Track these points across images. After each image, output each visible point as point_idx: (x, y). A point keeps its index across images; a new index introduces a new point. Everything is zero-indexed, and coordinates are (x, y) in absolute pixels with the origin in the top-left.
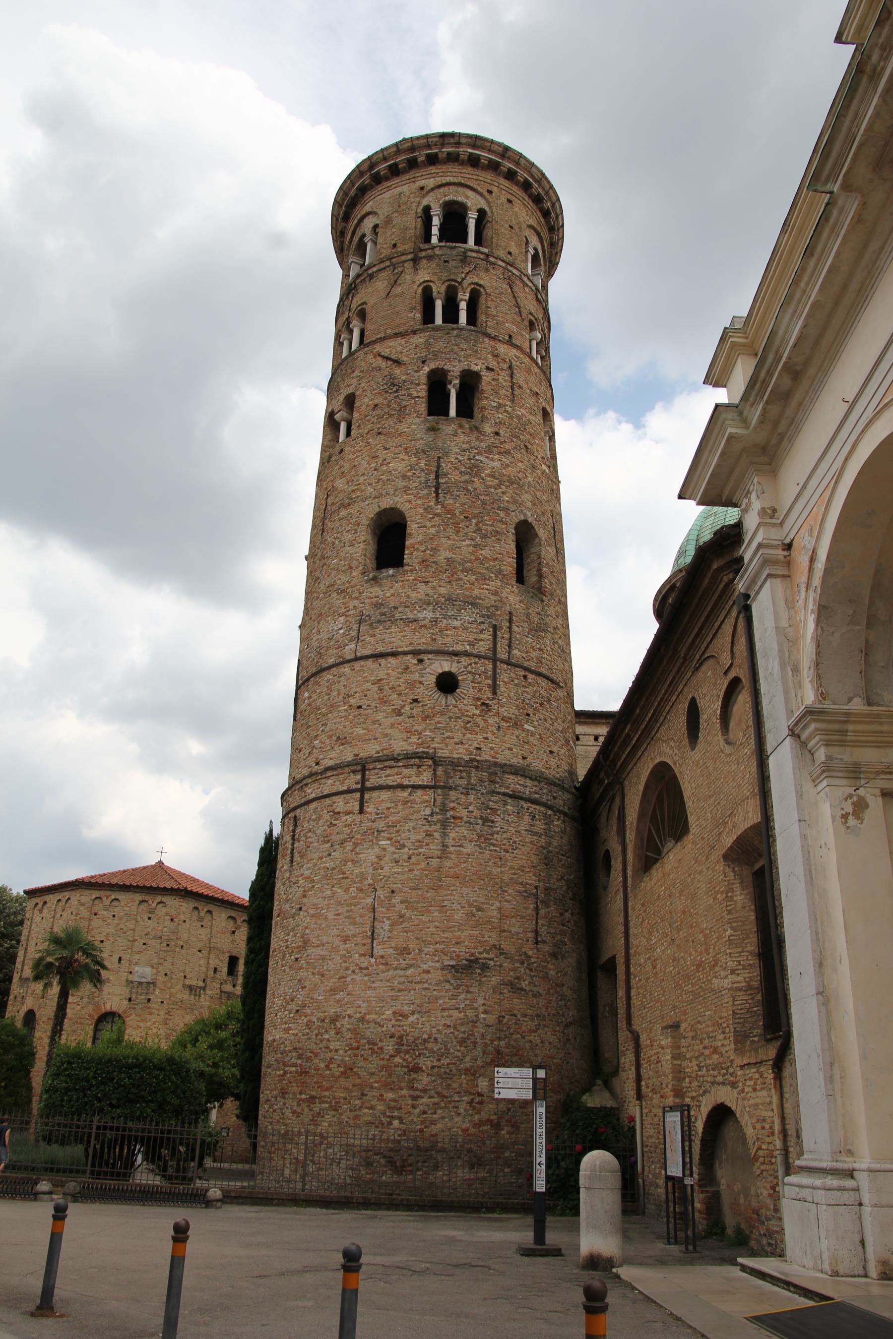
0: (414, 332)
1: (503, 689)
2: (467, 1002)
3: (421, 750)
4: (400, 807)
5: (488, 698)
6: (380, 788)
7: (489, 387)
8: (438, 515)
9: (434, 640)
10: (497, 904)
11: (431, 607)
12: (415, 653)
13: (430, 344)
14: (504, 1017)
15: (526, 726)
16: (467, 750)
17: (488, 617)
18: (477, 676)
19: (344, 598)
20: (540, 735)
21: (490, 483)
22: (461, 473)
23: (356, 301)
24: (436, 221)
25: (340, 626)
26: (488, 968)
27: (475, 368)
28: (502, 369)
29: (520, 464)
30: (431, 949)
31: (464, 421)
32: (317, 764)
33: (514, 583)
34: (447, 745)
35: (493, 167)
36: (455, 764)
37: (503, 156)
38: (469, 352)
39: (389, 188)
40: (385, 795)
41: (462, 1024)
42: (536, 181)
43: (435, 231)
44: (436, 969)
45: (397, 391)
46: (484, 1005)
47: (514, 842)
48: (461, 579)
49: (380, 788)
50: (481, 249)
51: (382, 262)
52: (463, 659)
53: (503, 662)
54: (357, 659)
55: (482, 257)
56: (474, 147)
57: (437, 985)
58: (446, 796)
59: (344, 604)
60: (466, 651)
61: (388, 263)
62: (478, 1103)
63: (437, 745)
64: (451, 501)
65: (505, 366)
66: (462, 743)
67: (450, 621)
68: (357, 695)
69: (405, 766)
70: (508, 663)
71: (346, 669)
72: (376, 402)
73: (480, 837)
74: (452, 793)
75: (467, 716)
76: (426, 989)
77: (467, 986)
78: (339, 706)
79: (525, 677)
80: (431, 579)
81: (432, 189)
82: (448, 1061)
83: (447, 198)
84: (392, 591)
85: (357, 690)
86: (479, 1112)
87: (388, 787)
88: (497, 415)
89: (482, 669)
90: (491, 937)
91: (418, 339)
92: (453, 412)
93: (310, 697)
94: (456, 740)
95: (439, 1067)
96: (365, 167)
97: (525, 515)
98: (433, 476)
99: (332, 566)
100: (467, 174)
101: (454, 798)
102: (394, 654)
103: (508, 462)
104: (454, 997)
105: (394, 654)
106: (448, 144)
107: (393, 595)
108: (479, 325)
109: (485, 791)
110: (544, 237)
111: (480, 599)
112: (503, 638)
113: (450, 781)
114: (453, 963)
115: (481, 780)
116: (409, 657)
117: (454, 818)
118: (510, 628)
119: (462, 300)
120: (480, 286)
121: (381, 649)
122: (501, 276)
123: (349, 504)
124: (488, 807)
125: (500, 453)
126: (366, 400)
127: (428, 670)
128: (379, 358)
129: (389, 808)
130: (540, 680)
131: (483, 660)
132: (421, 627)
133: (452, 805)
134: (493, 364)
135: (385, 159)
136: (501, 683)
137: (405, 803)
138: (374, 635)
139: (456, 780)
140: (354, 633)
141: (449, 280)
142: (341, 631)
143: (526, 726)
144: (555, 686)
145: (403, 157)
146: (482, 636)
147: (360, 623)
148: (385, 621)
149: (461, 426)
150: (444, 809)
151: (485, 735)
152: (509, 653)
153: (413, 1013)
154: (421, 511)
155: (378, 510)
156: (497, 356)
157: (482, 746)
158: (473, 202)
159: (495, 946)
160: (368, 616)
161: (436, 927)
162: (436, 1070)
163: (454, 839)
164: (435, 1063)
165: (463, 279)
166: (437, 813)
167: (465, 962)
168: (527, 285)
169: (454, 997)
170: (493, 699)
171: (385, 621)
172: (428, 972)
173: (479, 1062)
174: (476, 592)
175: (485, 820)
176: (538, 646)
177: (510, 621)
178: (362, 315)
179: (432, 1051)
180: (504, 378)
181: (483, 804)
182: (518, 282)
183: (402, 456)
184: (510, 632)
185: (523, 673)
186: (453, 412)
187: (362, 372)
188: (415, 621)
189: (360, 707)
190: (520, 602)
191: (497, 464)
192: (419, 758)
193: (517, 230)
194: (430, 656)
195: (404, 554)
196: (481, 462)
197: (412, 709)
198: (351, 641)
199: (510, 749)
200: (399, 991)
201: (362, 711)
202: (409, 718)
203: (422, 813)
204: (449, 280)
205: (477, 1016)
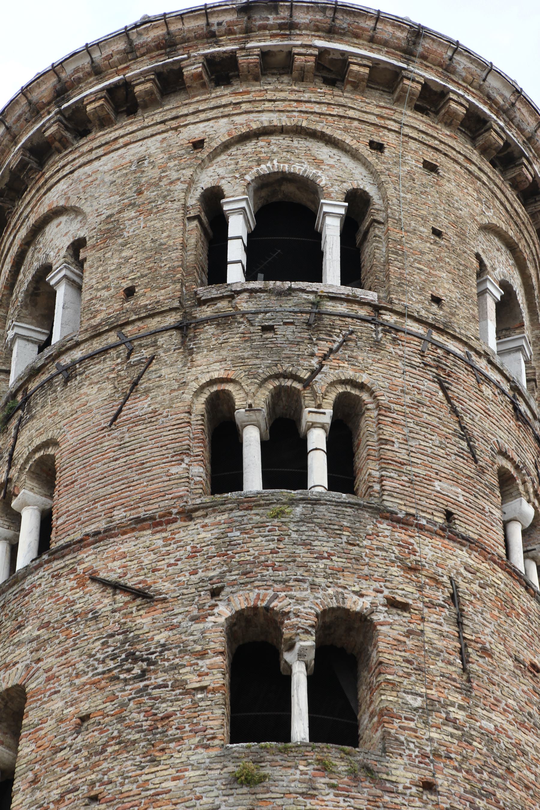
0: (188, 515)
7: (398, 656)
27: (356, 604)
31: (332, 752)
35: (385, 81)
37: (408, 53)
38: (338, 562)
42: (500, 111)
43: (236, 251)
50: (359, 292)
55: (363, 312)
56: (331, 32)
61: (112, 338)
65: (441, 596)
72: (84, 707)
81: (226, 146)
83: (264, 169)
91: (200, 533)
92: (300, 728)
96: (44, 93)
100: (311, 104)
106: (264, 27)
119: (313, 425)
120: (362, 386)
122: (417, 360)
126: (57, 704)
128: (93, 587)
134: (406, 591)
135: (97, 72)
141: (276, 376)
145: (145, 65)
149: (325, 768)
158: (334, 175)
165: (314, 373)
168: (488, 380)
180: (437, 627)
186: (300, 728)
193: (454, 240)
204: (276, 376)
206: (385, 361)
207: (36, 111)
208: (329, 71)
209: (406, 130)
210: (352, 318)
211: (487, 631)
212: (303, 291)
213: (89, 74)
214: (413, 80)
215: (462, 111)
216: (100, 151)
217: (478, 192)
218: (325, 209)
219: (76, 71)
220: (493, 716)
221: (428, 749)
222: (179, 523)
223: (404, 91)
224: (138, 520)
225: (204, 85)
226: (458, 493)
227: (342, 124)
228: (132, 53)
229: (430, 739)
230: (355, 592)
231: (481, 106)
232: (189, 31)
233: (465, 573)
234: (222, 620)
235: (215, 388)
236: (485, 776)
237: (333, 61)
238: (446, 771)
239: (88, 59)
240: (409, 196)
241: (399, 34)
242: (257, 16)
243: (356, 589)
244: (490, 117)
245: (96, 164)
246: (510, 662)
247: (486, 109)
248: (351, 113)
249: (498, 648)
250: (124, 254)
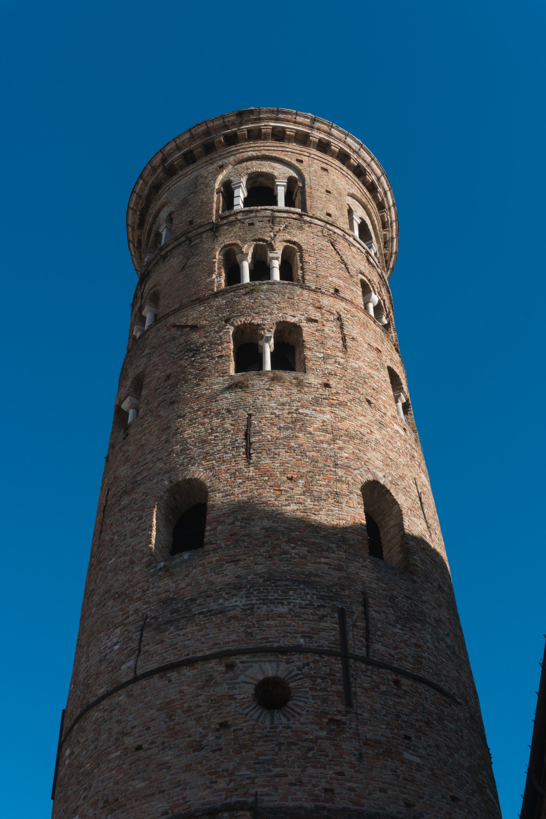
1: (362, 699)
3: (234, 799)
5: (339, 712)
8: (249, 479)
9: (249, 634)
11: (243, 592)
15: (407, 756)
18: (319, 680)
19: (123, 602)
20: (431, 769)
21: (322, 438)
22: (280, 428)
23: (149, 284)
25: (115, 640)
28: (327, 320)
29: (361, 418)
33: (367, 555)
34: (276, 788)
39: (183, 176)
42: (354, 151)
48: (287, 553)
50: (292, 209)
51: (177, 239)
52: (295, 657)
53: (358, 659)
54: (136, 679)
55: (295, 216)
60: (300, 646)
61: (183, 239)
63: (260, 790)
64: (268, 461)
67: (272, 607)
68: (135, 730)
70: (367, 661)
71: (121, 698)
72: (168, 372)
75: (306, 740)
78: (109, 754)
79: (397, 682)
80: (243, 557)
84: (188, 580)
85: (136, 723)
88: (324, 366)
89: (327, 670)
92: (268, 366)
93: (72, 753)
96: (157, 161)
97: (374, 474)
98: (241, 436)
99: (108, 568)
102: (190, 662)
103: (343, 414)
105: (190, 662)
107: (189, 585)
108: (295, 279)
110: (372, 211)
111: (317, 575)
112: (355, 626)
116: (213, 664)
118: (365, 613)
121: (171, 658)
122: (320, 234)
123: (133, 489)
125: (331, 405)
126: (157, 374)
127: (242, 678)
128: (173, 330)
130: (421, 688)
131: (326, 658)
134: (316, 315)
136: (358, 690)
140: (134, 645)
142: (117, 647)
143: (407, 756)
144: (448, 700)
145: (199, 142)
146: (322, 624)
147: (142, 630)
148: (178, 620)
151: (338, 769)
152: (368, 647)
156: (320, 308)
168: (354, 246)
170: (347, 712)
171: (178, 620)
174: (310, 568)
176: (413, 641)
177: (365, 604)
178: (155, 298)
182: (342, 241)
184: (367, 619)
185: (394, 676)
186: (268, 366)
188: (221, 612)
190: (378, 579)
191: (328, 416)
193: (336, 195)
194: (244, 658)
195: (204, 531)
196: (307, 415)
197: (218, 738)
198: (129, 656)
199: (382, 790)
201: (142, 754)
202: (214, 751)
206: (305, 234)
208: (278, 136)
209: (313, 156)
210: (290, 218)
211: (354, 332)
212: (267, 210)
213: (175, 150)
214: (314, 137)
216: (180, 178)
217: (347, 181)
218: (277, 183)
219: (170, 150)
220: (357, 362)
221: (326, 372)
223: (311, 141)
224: (192, 301)
225: (223, 146)
227: (284, 153)
228: (193, 138)
230: (291, 316)
231: (346, 149)
232: (216, 125)
233: (344, 311)
235: (227, 248)
236: (353, 382)
237: (278, 131)
238: (334, 380)
239: (175, 144)
240: (315, 178)
242: (244, 116)
243: (292, 314)
244: (349, 154)
245: (179, 183)
246: (366, 345)
247: (348, 150)
248: (288, 150)
249: (360, 339)
250: (189, 210)
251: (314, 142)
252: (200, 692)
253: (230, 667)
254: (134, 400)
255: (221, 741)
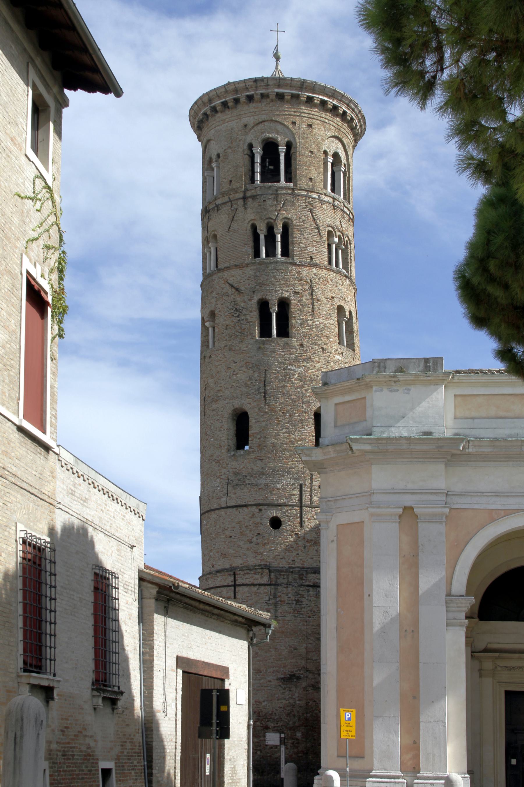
0: (247, 265)
1: (306, 523)
2: (290, 696)
4: (253, 596)
6: (243, 585)
10: (305, 645)
12: (257, 505)
13: (257, 276)
14: (309, 702)
16: (287, 562)
17: (297, 479)
24: (258, 159)
26: (300, 678)
27: (286, 295)
30: (272, 670)
32: (213, 566)
34: (276, 560)
36: (279, 571)
40: (246, 589)
41: (287, 706)
43: (258, 168)
44: (274, 680)
45: (238, 316)
46: (298, 697)
47: (314, 612)
49: (243, 585)
55: (289, 191)
56: (279, 86)
57: (275, 687)
58: (276, 589)
59: (219, 470)
62: (296, 743)
65: (307, 287)
66: (284, 558)
68: (229, 530)
69: (255, 573)
71: (222, 512)
73: (294, 611)
74: (279, 587)
76: (269, 689)
77: (289, 688)
82: (281, 724)
85: (229, 526)
86: (297, 747)
87: (247, 585)
90: (303, 663)
91: (250, 271)
94: (281, 557)
95: (277, 727)
96: (206, 99)
101: (280, 590)
102: (246, 506)
104: (283, 693)
105: (246, 506)
107: (244, 467)
109: (297, 585)
113: (278, 581)
114: (282, 676)
115: (295, 579)
116: (255, 508)
117: (281, 601)
118: (311, 483)
120: (289, 219)
121: (239, 503)
124: (299, 594)
127: (264, 516)
129: (248, 597)
132: (260, 489)
133: (279, 594)
134: (298, 288)
135: (218, 97)
137: (256, 594)
138: (235, 494)
139: (281, 580)
142: (219, 488)
148: (241, 485)
150: (275, 597)
151: (297, 552)
153: (264, 702)
154: (256, 410)
155: (233, 408)
157: (296, 559)
159: (304, 667)
160: (231, 480)
161: (273, 659)
162: (276, 728)
163: (281, 613)
164: (276, 725)
166: (272, 599)
167: (288, 676)
169: (283, 693)
171: (241, 485)
172: (270, 681)
173: (297, 724)
175: (297, 601)
179: (274, 719)
181: (296, 592)
183: (244, 369)
187: (218, 294)
189: (231, 537)
191: (301, 370)
192: (262, 568)
194: (265, 507)
197: (257, 539)
199: (312, 558)
200: (257, 690)
203: (264, 599)
205: (295, 702)
207: (204, 104)
215: (319, 102)
222: (245, 268)
224: (236, 266)
226: (314, 250)
228: (226, 92)
229: (303, 332)
234: (255, 301)
241: (298, 83)
251: (303, 102)
252: (250, 519)
253: (260, 510)
254: (211, 323)
255: (258, 541)
